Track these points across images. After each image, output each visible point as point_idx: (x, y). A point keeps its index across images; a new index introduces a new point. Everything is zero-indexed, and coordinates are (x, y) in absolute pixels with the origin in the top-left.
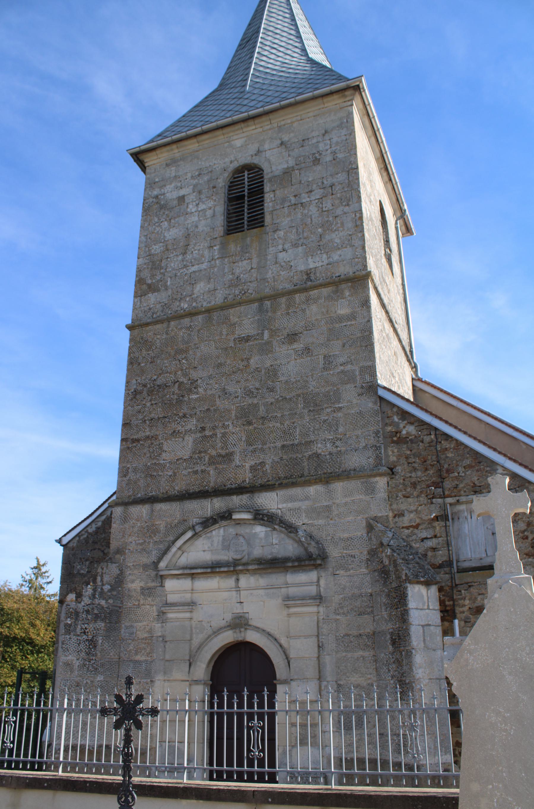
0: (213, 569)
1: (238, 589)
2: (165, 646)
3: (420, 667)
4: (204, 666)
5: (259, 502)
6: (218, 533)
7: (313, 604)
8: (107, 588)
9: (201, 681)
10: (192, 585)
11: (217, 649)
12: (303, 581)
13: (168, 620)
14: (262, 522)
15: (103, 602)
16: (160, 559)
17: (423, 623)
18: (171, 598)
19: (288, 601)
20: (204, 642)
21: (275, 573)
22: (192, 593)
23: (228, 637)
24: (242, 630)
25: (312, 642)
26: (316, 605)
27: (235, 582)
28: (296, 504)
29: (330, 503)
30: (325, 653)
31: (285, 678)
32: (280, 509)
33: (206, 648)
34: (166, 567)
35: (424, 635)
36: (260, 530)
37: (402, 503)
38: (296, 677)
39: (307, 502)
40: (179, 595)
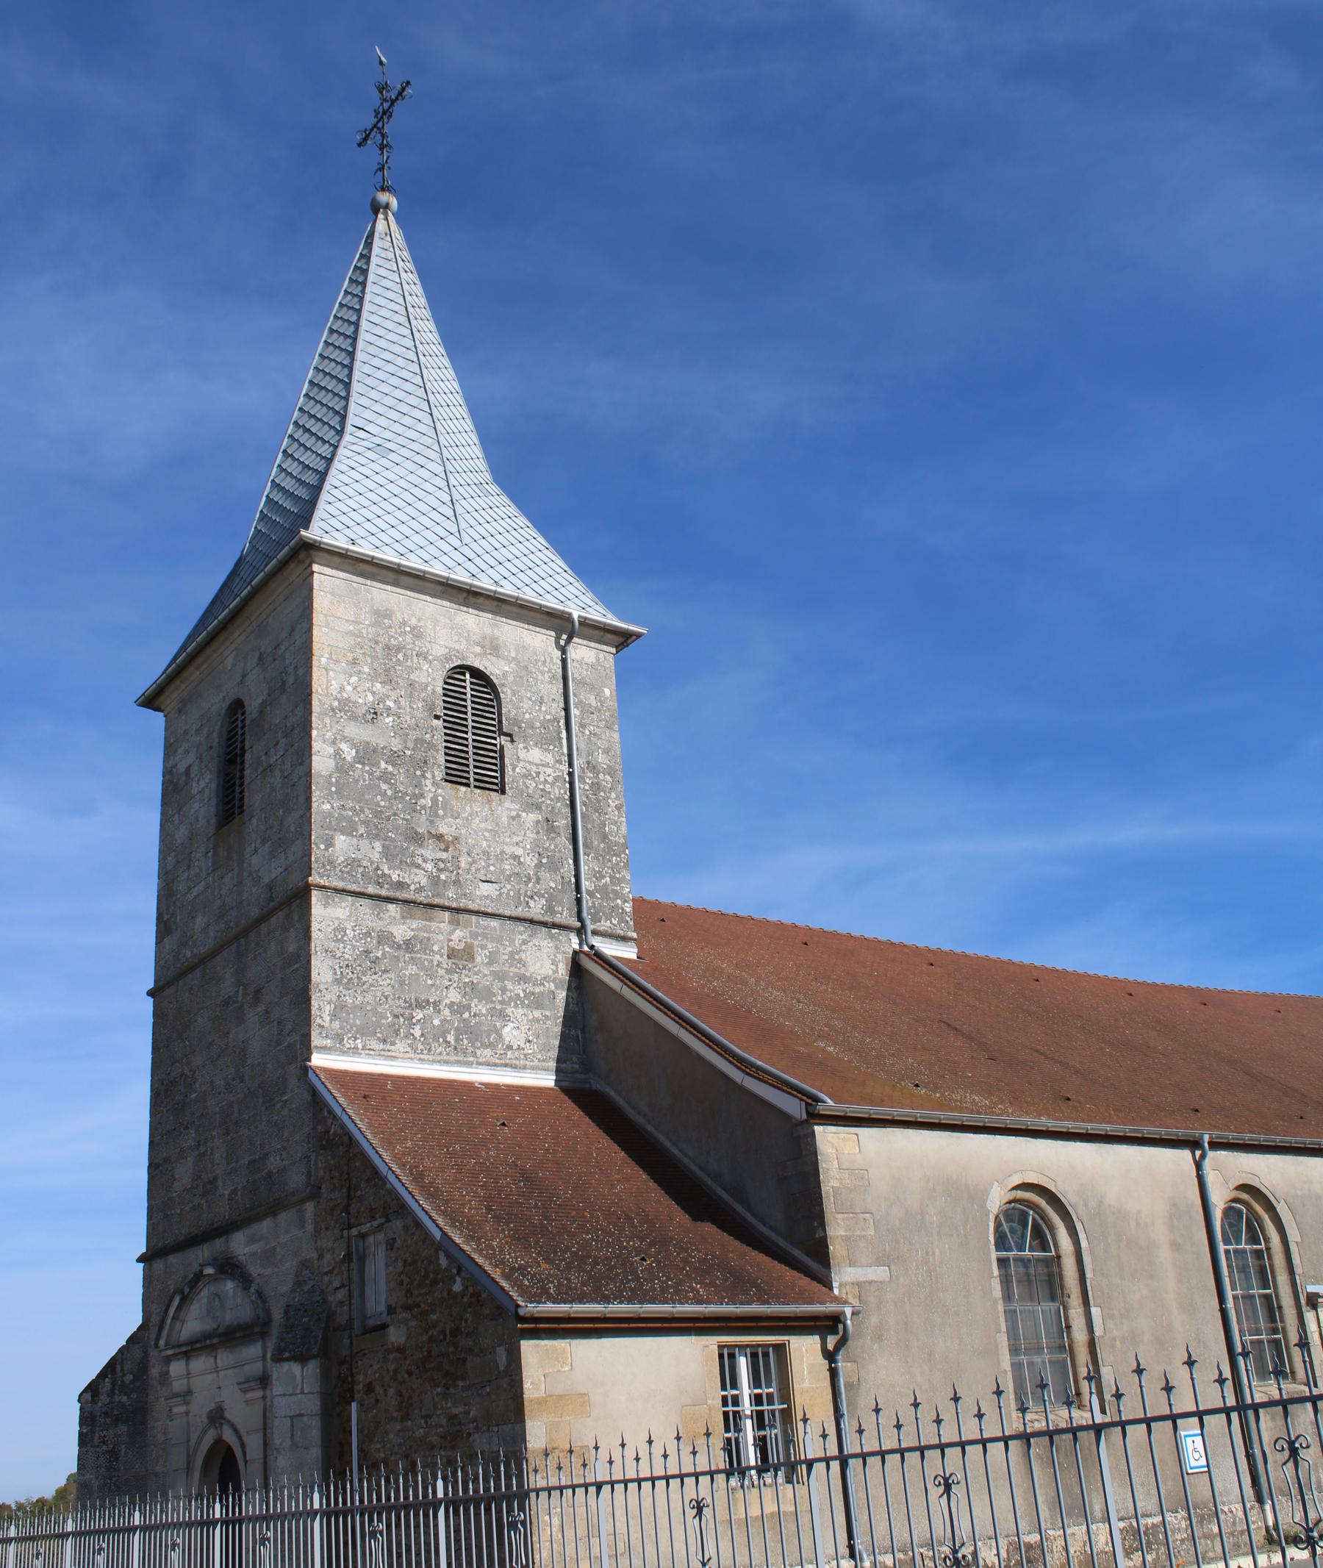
3: (283, 1473)
8: (129, 1378)
15: (124, 1399)
17: (292, 1413)
35: (292, 1431)
37: (327, 1229)
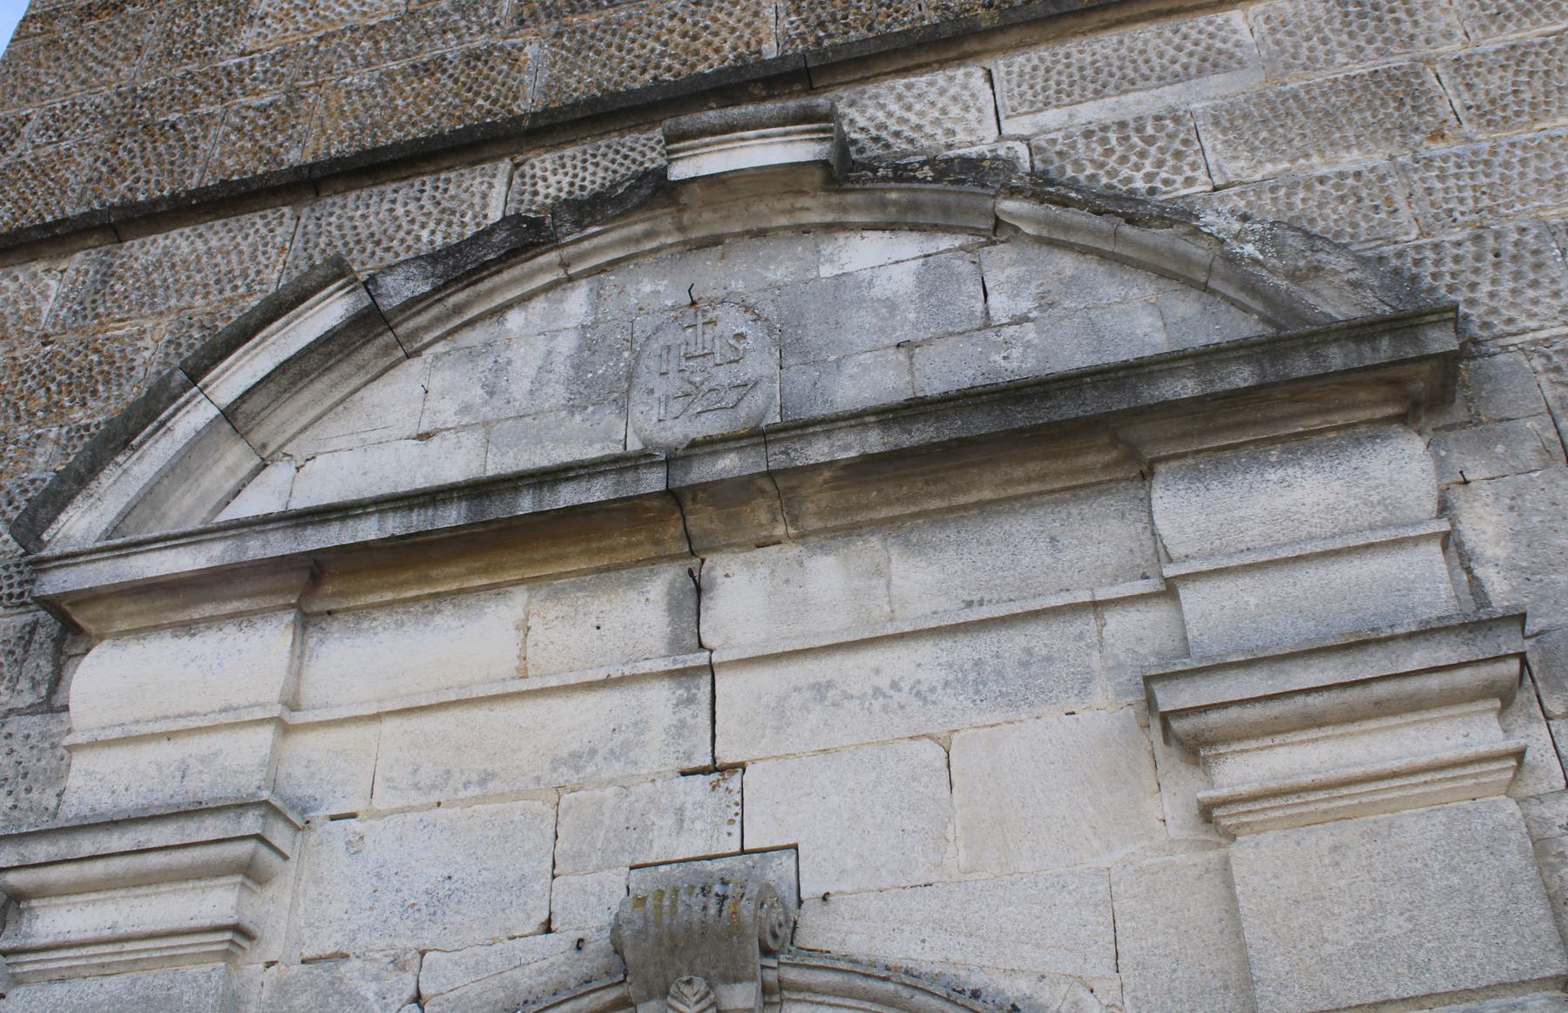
0: (484, 533)
1: (696, 670)
5: (862, 122)
12: (1307, 528)
16: (74, 481)
22: (285, 729)
26: (1487, 691)
27: (674, 608)
32: (1021, 138)
34: (114, 530)
40: (167, 752)
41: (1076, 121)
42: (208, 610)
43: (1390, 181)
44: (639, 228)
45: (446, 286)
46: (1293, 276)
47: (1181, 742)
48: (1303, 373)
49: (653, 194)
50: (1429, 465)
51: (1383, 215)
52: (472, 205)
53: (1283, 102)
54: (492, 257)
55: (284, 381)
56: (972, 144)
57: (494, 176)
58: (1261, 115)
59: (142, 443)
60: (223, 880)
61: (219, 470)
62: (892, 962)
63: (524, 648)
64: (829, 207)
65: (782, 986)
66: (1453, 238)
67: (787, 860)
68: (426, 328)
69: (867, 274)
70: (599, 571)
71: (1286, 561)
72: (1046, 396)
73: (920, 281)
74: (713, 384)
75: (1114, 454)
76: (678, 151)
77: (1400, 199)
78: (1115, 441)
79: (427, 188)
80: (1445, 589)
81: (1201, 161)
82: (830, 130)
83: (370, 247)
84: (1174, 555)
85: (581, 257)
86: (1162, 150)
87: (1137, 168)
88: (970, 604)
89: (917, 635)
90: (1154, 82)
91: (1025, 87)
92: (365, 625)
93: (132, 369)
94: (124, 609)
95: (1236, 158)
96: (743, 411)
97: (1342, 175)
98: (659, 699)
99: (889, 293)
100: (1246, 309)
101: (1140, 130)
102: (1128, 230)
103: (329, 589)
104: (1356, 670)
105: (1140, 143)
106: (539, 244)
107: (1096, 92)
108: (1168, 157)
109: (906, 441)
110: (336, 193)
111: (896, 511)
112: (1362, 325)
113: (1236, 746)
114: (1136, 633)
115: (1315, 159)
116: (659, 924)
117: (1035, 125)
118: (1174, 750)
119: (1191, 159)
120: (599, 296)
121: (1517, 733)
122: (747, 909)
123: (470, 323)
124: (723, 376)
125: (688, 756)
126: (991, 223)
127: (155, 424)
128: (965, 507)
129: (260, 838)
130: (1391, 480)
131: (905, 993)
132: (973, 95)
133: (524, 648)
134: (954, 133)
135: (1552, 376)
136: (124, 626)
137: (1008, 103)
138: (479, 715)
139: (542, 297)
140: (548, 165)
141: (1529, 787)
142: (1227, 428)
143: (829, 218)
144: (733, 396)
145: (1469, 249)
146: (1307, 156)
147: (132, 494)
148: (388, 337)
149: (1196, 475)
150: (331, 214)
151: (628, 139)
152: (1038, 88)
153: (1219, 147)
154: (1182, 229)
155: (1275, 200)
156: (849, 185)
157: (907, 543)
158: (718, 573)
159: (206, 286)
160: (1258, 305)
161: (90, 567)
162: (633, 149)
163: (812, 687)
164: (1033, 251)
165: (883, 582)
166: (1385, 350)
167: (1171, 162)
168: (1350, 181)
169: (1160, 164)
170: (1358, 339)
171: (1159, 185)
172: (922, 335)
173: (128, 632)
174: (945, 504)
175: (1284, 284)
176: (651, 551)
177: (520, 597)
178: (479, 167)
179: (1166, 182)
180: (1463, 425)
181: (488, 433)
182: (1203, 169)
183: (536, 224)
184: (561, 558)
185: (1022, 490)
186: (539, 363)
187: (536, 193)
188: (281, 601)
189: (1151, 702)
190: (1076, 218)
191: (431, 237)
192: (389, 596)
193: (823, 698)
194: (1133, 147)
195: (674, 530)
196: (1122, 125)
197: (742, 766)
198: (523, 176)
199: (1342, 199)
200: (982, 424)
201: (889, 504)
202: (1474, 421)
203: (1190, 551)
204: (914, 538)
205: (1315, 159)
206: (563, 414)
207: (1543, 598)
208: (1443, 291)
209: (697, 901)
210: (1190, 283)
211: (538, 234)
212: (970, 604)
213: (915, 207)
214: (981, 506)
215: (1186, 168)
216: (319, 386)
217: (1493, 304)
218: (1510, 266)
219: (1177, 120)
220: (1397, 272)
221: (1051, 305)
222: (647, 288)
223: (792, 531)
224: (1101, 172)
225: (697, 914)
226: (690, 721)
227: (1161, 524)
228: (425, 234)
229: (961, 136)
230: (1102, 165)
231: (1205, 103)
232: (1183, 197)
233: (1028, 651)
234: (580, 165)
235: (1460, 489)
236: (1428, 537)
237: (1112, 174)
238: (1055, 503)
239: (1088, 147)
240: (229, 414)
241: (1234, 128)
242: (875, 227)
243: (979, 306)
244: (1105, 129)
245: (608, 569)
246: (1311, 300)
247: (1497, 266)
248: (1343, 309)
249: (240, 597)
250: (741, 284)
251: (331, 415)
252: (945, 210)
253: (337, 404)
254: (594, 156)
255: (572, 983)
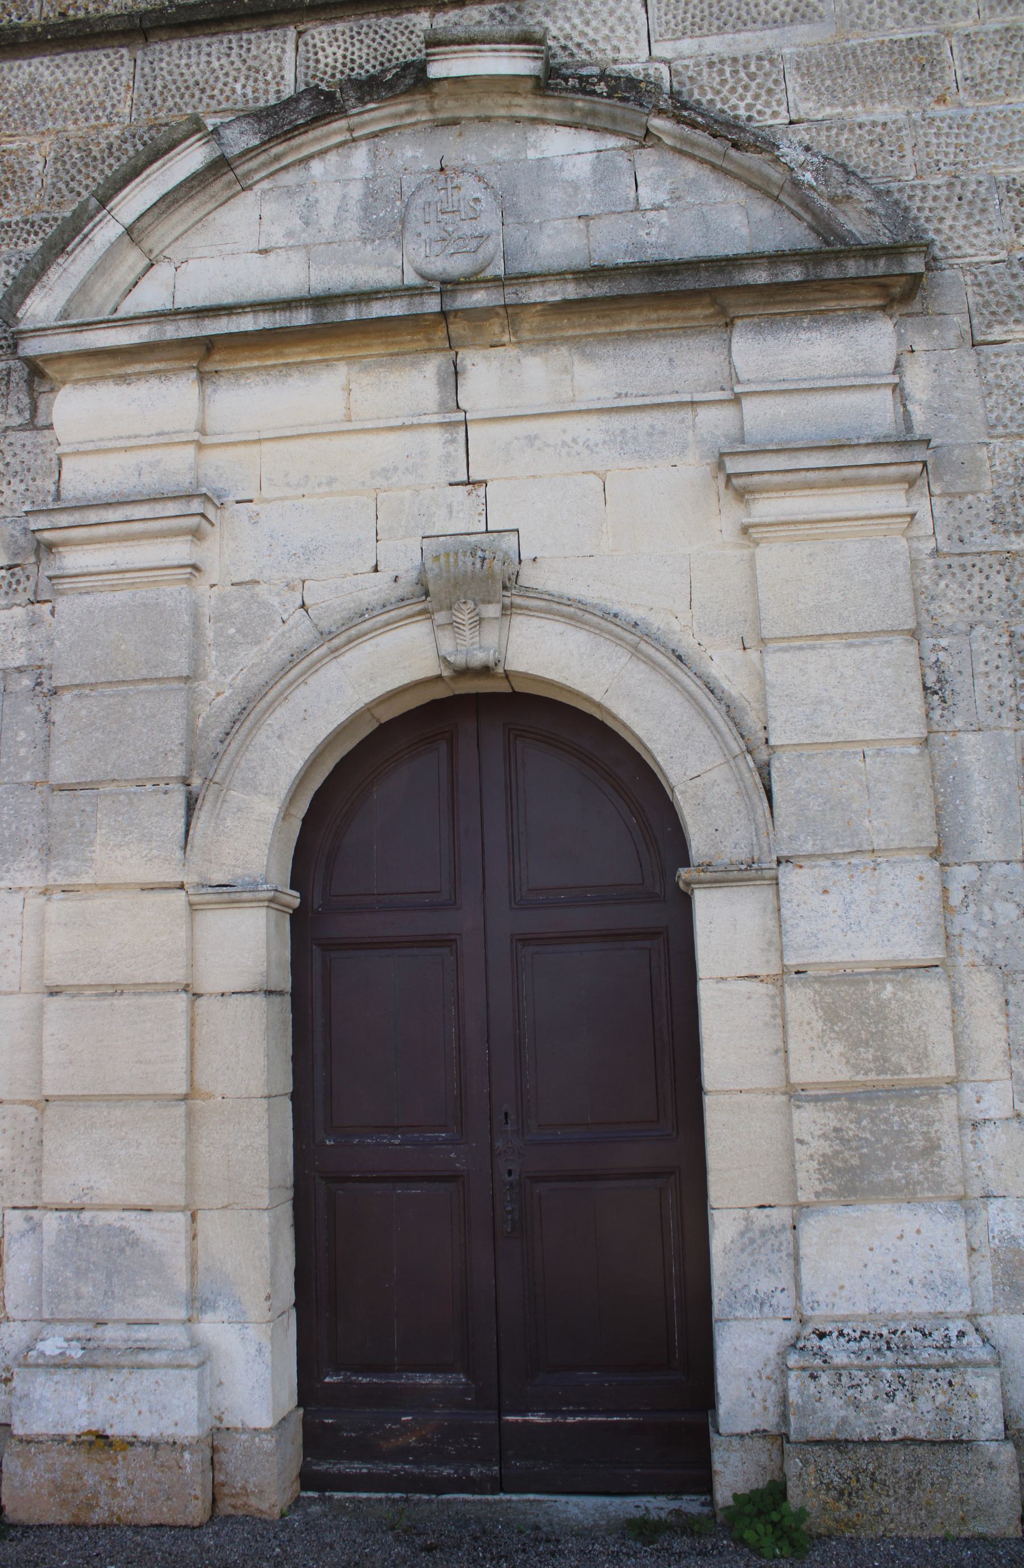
0: (320, 325)
1: (458, 423)
2: (47, 718)
4: (269, 808)
5: (554, 32)
6: (338, 173)
7: (892, 470)
9: (253, 887)
10: (203, 410)
11: (342, 717)
12: (821, 367)
13: (66, 584)
14: (581, 103)
18: (81, 477)
19: (734, 475)
20: (268, 685)
21: (657, 334)
22: (200, 446)
23: (404, 658)
24: (492, 610)
25: (894, 667)
27: (442, 383)
28: (750, 41)
29: (928, 31)
30: (959, 723)
31: (742, 854)
32: (664, 61)
33: (281, 716)
34: (65, 314)
36: (567, 149)
38: (809, 848)
39: (803, 29)
40: (129, 459)
41: (703, 52)
42: (137, 368)
43: (904, 132)
44: (403, 108)
45: (270, 140)
46: (833, 200)
47: (735, 490)
48: (831, 276)
49: (415, 85)
50: (894, 340)
51: (895, 159)
52: (271, 66)
53: (845, 57)
54: (302, 121)
55: (163, 207)
56: (631, 61)
57: (285, 42)
58: (829, 66)
59: (74, 250)
60: (180, 539)
61: (123, 269)
62: (571, 596)
63: (348, 402)
64: (535, 106)
65: (512, 605)
66: (936, 183)
67: (513, 537)
68: (256, 170)
69: (559, 160)
70: (391, 355)
71: (805, 390)
72: (677, 273)
73: (594, 171)
74: (460, 233)
75: (711, 310)
76: (434, 54)
77: (908, 151)
78: (714, 303)
79: (234, 45)
80: (890, 417)
81: (784, 99)
82: (542, 52)
83: (197, 93)
84: (741, 379)
85: (363, 125)
86: (760, 86)
87: (742, 98)
88: (619, 395)
89: (588, 411)
90: (759, 25)
91: (670, 16)
92: (242, 381)
93: (32, 179)
94: (80, 366)
95: (807, 99)
96: (480, 255)
97: (874, 124)
98: (435, 438)
99: (573, 177)
100: (800, 218)
101: (746, 67)
102: (733, 152)
103: (217, 357)
104: (835, 457)
105: (745, 78)
106: (333, 114)
107: (719, 28)
108: (763, 92)
109: (591, 293)
110: (161, 40)
111: (578, 332)
112: (871, 249)
113: (765, 495)
114: (715, 421)
115: (859, 108)
116: (448, 571)
117: (675, 50)
118: (730, 493)
119: (777, 97)
120: (376, 156)
121: (914, 502)
122: (497, 565)
123: (285, 168)
124: (466, 228)
125: (454, 474)
126: (644, 132)
127: (81, 236)
128: (619, 333)
129: (203, 515)
130: (871, 347)
131: (580, 613)
132: (633, 18)
133: (348, 402)
134: (619, 51)
135: (975, 288)
136: (80, 376)
137: (657, 29)
138: (323, 442)
139: (334, 152)
140: (324, 36)
141: (915, 532)
142: (781, 302)
143: (535, 114)
144: (474, 243)
145: (944, 192)
146: (854, 104)
147: (74, 287)
148: (230, 176)
149: (758, 329)
150: (161, 60)
151: (383, 21)
152: (679, 18)
153: (798, 89)
154: (768, 157)
155: (828, 137)
156: (550, 93)
157: (583, 353)
158: (468, 362)
159: (73, 113)
160: (808, 217)
161: (56, 338)
162: (387, 32)
163: (526, 437)
164: (669, 156)
165: (569, 377)
166: (881, 266)
167: (764, 98)
168: (879, 129)
169: (757, 97)
170: (867, 258)
171: (755, 115)
172: (595, 211)
173: (82, 380)
174: (608, 331)
175: (826, 204)
176: (425, 345)
177: (342, 368)
178: (272, 32)
179: (759, 113)
180: (917, 314)
181: (308, 253)
182: (785, 106)
183: (330, 96)
184: (368, 346)
185: (654, 326)
186: (338, 203)
187: (317, 61)
188: (186, 364)
189: (720, 466)
190: (701, 139)
191: (243, 91)
192: (256, 363)
193: (532, 445)
194: (740, 80)
195: (441, 334)
196: (735, 60)
197: (485, 483)
198: (306, 44)
199: (871, 143)
200: (637, 286)
201: (574, 327)
202: (924, 313)
203: (751, 377)
204: (588, 350)
205: (859, 108)
206: (359, 243)
207: (942, 427)
208: (922, 221)
209: (469, 560)
210: (767, 194)
211: (332, 105)
212: (619, 395)
213: (594, 114)
214: (630, 334)
215: (774, 103)
216: (186, 209)
217: (951, 234)
218: (966, 208)
219: (772, 61)
220: (897, 203)
221: (678, 198)
222: (409, 154)
223: (513, 339)
224: (717, 99)
225: (470, 568)
226: (453, 453)
227: (735, 358)
228: (238, 87)
229: (624, 54)
230: (718, 92)
231: (793, 50)
232: (771, 126)
233: (652, 427)
234: (349, 40)
235: (909, 355)
236: (886, 385)
237: (724, 101)
238: (673, 336)
239: (710, 75)
240: (129, 231)
241: (809, 74)
242: (565, 124)
243: (632, 194)
244: (722, 61)
245: (397, 354)
246: (842, 219)
247: (958, 206)
248: (860, 227)
249: (159, 361)
250: (474, 158)
251: (193, 230)
252: (614, 119)
253: (197, 222)
254: (359, 33)
255: (393, 600)
